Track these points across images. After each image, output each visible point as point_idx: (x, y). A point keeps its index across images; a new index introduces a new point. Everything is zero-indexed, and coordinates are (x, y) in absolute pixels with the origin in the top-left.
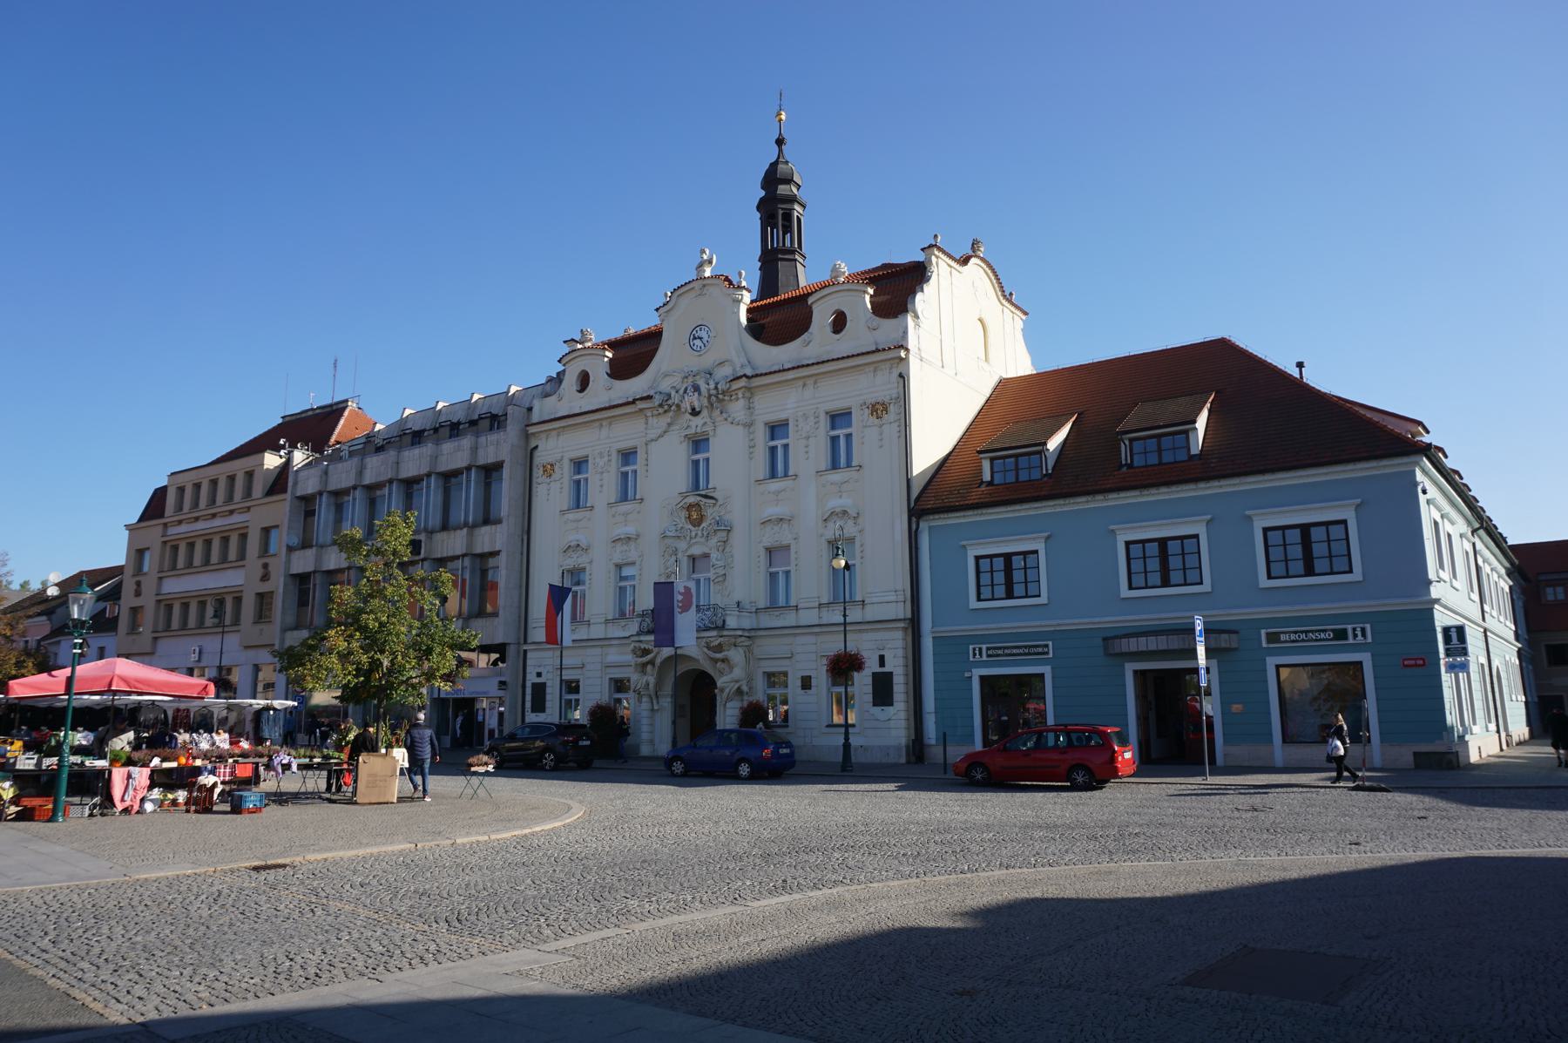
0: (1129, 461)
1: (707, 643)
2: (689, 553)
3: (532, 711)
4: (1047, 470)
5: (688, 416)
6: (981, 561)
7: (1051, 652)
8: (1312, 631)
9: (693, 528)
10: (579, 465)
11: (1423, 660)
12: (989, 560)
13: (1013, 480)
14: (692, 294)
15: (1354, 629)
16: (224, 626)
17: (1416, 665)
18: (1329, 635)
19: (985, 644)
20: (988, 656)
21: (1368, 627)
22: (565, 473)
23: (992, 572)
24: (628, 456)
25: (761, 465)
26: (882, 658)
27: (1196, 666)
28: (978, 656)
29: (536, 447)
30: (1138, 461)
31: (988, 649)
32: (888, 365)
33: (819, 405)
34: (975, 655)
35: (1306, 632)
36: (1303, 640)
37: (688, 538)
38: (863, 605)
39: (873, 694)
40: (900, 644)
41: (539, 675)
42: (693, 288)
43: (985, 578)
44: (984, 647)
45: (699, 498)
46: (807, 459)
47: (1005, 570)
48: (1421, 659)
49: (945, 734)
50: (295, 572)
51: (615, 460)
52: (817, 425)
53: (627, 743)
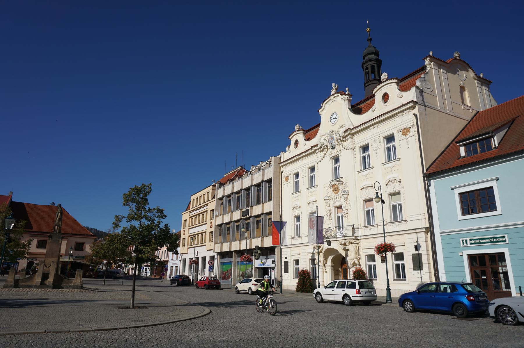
1: (340, 243)
2: (335, 205)
3: (284, 273)
4: (495, 145)
5: (331, 150)
9: (335, 195)
10: (297, 175)
14: (331, 101)
16: (195, 245)
20: (471, 244)
21: (462, 245)
22: (292, 179)
24: (312, 169)
25: (358, 165)
28: (465, 244)
29: (283, 171)
31: (470, 240)
33: (291, 172)
34: (463, 243)
37: (334, 199)
39: (413, 264)
41: (286, 258)
42: (330, 99)
44: (468, 239)
45: (336, 182)
46: (303, 185)
49: (520, 288)
50: (218, 224)
51: (383, 142)
52: (380, 144)
53: (40, 278)
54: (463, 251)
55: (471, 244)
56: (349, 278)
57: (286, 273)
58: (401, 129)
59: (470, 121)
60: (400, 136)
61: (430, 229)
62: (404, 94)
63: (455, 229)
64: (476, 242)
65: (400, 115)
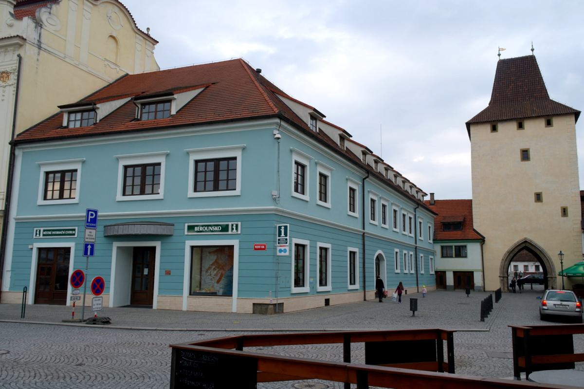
0: (139, 118)
6: (199, 164)
7: (76, 234)
8: (211, 226)
12: (152, 167)
15: (232, 225)
19: (231, 222)
20: (44, 235)
21: (239, 224)
23: (206, 172)
28: (38, 235)
30: (72, 126)
31: (44, 231)
34: (237, 226)
36: (206, 231)
43: (129, 181)
44: (42, 229)
54: (34, 244)
56: (287, 254)
62: (17, 23)
64: (50, 234)
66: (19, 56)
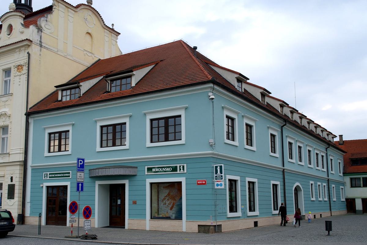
0: (109, 90)
8: (164, 167)
11: (205, 181)
13: (65, 100)
15: (180, 167)
17: (202, 184)
18: (170, 169)
20: (50, 177)
21: (185, 165)
26: (12, 178)
27: (109, 185)
30: (64, 100)
31: (50, 174)
32: (23, 48)
35: (162, 168)
36: (161, 172)
38: (9, 155)
39: (8, 193)
40: (18, 172)
43: (105, 137)
46: (19, 85)
47: (168, 126)
48: (204, 181)
54: (44, 183)
55: (50, 177)
57: (10, 200)
58: (16, 65)
59: (89, 68)
60: (15, 72)
61: (25, 163)
63: (44, 164)
64: (54, 176)
65: (17, 51)
66: (28, 53)
